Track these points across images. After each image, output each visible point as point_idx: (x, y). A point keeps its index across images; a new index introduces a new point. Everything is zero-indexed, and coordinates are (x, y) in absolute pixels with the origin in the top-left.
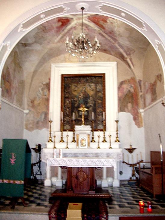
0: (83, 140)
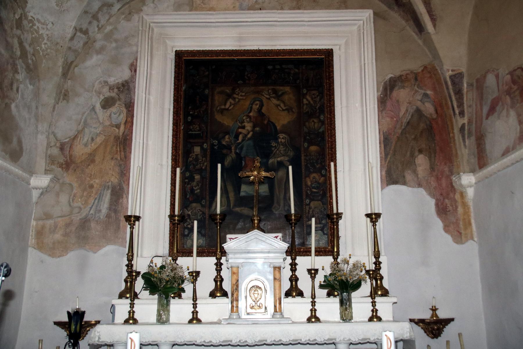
0: (258, 287)
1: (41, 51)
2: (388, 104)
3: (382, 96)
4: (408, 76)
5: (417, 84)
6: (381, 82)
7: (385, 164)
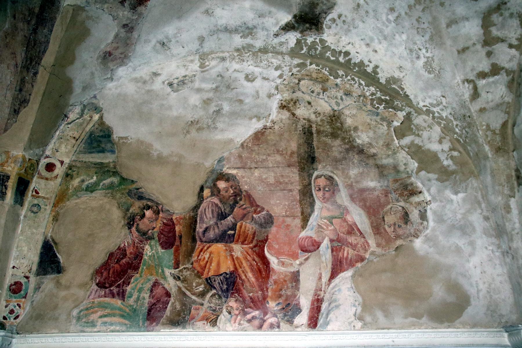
1: (459, 138)
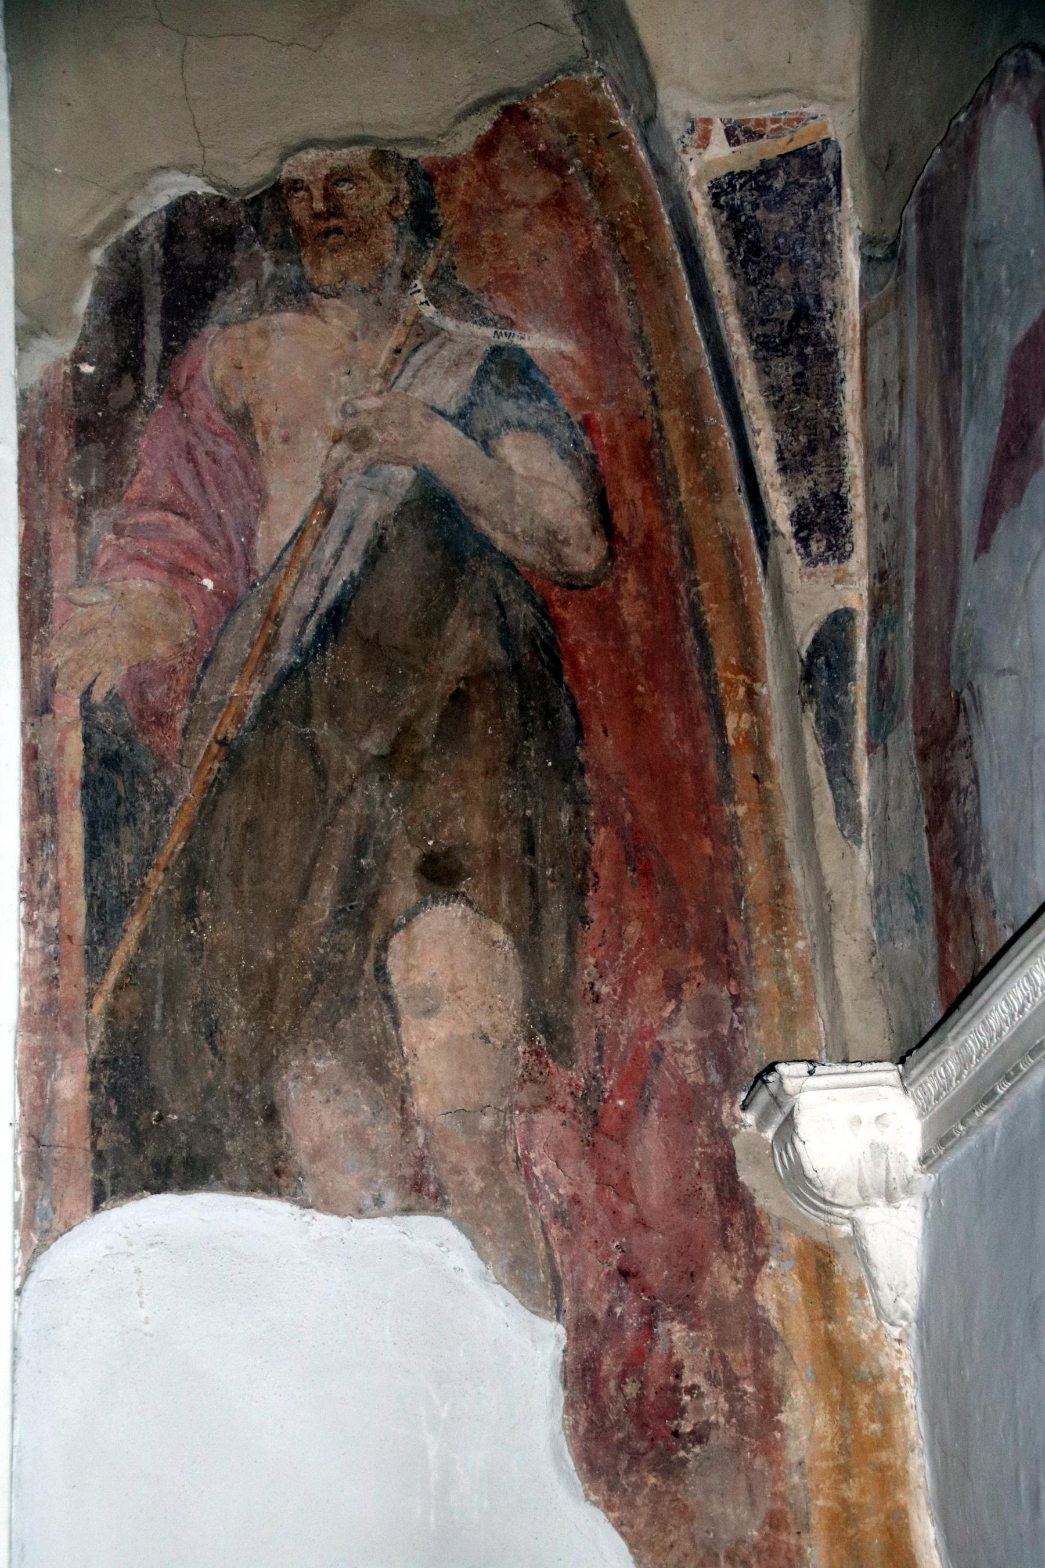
2: (143, 443)
3: (87, 369)
4: (344, 188)
5: (431, 264)
6: (88, 245)
7: (90, 996)
